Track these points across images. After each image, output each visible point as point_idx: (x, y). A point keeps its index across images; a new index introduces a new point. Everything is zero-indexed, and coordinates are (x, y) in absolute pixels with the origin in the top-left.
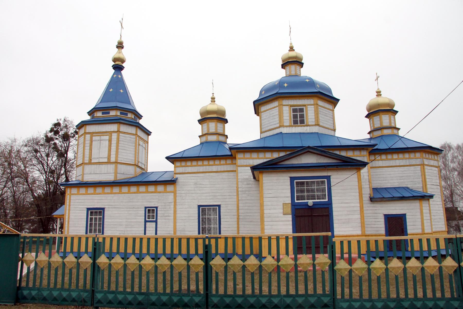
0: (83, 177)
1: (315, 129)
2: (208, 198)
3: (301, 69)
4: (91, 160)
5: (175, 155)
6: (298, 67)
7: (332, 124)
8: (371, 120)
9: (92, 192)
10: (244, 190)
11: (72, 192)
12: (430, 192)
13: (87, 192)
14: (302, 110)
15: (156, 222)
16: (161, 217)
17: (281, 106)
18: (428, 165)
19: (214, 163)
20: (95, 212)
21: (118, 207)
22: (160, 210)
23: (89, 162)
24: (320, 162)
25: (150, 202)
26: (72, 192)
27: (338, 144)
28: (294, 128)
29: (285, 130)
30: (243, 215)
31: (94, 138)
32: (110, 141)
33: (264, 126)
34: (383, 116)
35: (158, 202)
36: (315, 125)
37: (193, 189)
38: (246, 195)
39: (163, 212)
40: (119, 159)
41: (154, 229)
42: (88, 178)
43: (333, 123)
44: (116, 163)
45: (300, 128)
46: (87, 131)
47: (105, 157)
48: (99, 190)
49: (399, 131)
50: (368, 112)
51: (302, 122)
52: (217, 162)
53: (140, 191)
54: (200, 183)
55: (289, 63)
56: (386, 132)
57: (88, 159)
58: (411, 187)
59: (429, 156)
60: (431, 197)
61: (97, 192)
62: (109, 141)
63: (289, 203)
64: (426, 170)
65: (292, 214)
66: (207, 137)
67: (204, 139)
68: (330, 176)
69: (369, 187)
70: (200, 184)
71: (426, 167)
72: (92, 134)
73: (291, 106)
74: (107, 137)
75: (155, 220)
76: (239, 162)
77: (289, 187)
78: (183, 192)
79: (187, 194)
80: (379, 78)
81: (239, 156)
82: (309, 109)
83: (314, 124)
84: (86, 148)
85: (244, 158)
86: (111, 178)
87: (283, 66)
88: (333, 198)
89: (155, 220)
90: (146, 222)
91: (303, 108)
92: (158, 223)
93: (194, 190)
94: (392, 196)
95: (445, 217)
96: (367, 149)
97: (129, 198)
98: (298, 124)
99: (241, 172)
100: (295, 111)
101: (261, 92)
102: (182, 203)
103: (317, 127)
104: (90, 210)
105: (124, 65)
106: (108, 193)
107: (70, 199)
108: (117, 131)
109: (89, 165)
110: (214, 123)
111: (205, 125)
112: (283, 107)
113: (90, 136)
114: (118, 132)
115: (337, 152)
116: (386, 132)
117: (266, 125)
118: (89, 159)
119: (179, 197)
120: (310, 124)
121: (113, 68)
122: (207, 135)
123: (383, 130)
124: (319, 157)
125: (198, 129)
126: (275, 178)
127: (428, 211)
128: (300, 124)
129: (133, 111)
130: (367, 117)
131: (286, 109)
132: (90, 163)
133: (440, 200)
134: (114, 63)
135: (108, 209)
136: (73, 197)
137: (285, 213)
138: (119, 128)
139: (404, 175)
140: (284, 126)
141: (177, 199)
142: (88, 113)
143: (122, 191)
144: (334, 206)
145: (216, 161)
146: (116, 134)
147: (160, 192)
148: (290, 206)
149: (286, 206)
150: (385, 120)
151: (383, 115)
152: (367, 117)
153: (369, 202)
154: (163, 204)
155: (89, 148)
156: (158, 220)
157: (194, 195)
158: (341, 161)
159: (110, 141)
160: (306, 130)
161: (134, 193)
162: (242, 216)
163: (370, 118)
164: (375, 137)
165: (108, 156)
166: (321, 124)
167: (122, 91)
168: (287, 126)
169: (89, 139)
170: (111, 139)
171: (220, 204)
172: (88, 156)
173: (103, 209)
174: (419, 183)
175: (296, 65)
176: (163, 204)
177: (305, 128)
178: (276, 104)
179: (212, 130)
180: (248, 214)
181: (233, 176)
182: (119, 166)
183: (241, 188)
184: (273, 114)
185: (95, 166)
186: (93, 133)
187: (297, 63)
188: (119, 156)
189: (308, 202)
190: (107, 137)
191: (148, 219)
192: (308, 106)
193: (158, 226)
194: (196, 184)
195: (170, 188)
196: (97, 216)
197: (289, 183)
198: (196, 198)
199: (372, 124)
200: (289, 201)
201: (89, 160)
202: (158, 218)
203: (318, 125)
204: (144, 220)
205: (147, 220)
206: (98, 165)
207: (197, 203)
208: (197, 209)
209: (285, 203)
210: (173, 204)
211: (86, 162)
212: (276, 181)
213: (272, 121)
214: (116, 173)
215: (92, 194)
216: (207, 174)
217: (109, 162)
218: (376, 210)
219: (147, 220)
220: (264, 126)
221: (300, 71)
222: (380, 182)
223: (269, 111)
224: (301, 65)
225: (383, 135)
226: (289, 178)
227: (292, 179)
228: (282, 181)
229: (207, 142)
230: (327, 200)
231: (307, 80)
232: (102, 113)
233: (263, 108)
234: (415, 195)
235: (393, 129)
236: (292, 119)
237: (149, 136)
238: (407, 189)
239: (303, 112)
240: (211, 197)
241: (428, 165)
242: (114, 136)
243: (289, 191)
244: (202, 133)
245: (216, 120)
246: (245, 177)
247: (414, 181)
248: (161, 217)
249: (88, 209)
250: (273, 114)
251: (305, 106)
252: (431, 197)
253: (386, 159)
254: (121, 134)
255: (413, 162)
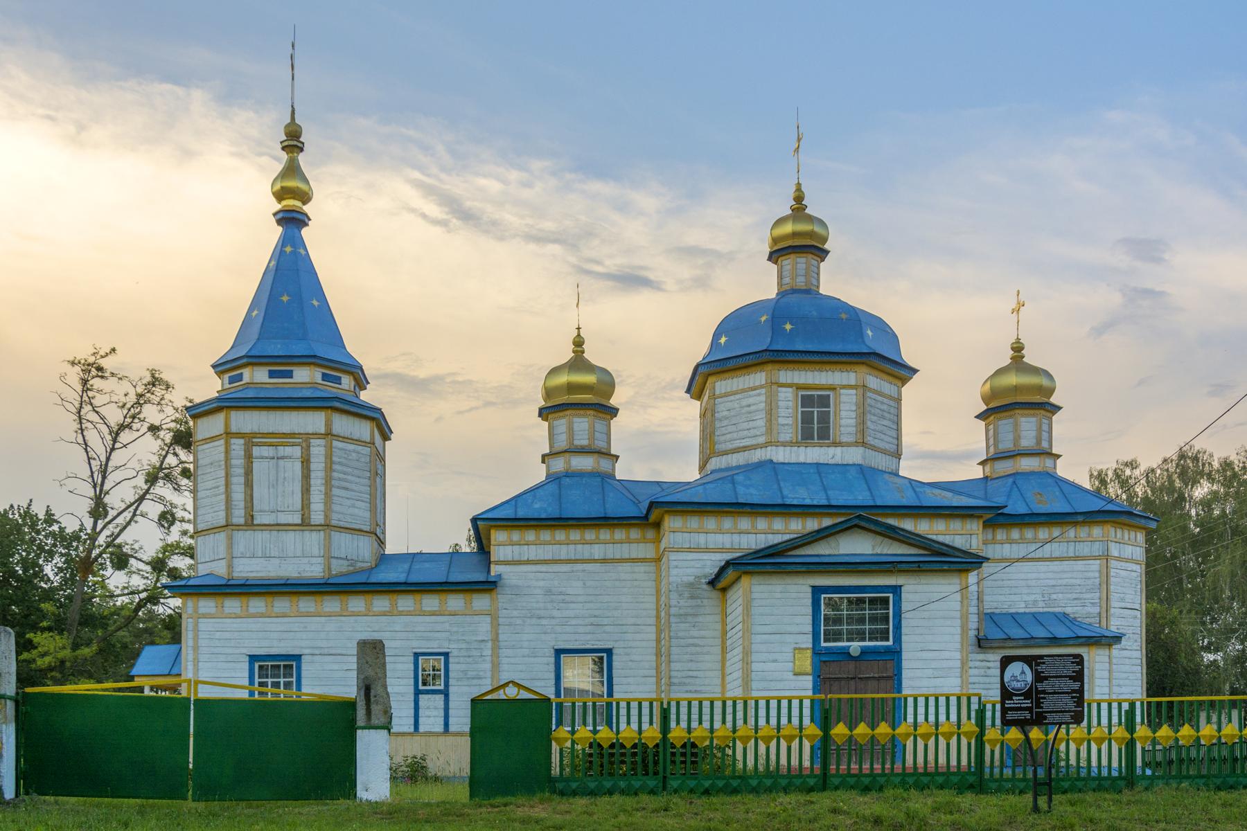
0: (230, 566)
1: (854, 455)
2: (581, 629)
3: (822, 264)
4: (252, 516)
5: (495, 511)
6: (812, 260)
7: (893, 438)
8: (991, 427)
9: (263, 610)
10: (682, 612)
11: (202, 611)
12: (1115, 626)
13: (247, 610)
14: (825, 402)
15: (447, 695)
16: (458, 679)
17: (774, 387)
18: (1119, 559)
19: (568, 537)
20: (284, 666)
21: (339, 651)
22: (456, 660)
23: (246, 522)
24: (885, 552)
25: (428, 639)
26: (202, 611)
27: (908, 499)
28: (802, 449)
29: (780, 455)
30: (679, 674)
31: (256, 451)
32: (306, 462)
33: (722, 438)
34: (1023, 419)
35: (450, 640)
36: (856, 444)
37: (541, 605)
38: (687, 625)
39: (463, 667)
40: (335, 516)
41: (442, 713)
42: (249, 569)
43: (896, 436)
44: (327, 526)
45: (817, 449)
46: (234, 429)
47: (295, 509)
48: (281, 604)
49: (1059, 461)
50: (987, 405)
51: (824, 434)
52: (605, 534)
53: (400, 609)
54: (560, 590)
55: (790, 251)
56: (1027, 464)
57: (242, 512)
58: (1074, 613)
59: (1123, 535)
60: (1117, 639)
61: (276, 610)
62: (302, 462)
63: (808, 649)
64: (1112, 570)
65: (813, 674)
66: (569, 460)
67: (559, 465)
68: (901, 586)
69: (976, 612)
70: (561, 594)
71: (1113, 563)
72: (251, 439)
73: (799, 387)
74: (297, 451)
75: (442, 687)
76: (669, 539)
77: (809, 610)
78: (515, 613)
79: (526, 619)
80: (1022, 308)
81: (670, 523)
82: (843, 398)
83: (851, 439)
84: (234, 480)
85: (685, 530)
86: (314, 570)
87: (774, 256)
88: (904, 638)
89: (442, 687)
90: (417, 693)
91: (829, 396)
92: (451, 695)
93: (546, 609)
94: (1029, 636)
95: (1145, 689)
96: (979, 517)
97: (368, 626)
98: (813, 439)
99: (677, 567)
100: (807, 401)
101: (717, 336)
102: (514, 643)
103: (860, 450)
104: (259, 661)
105: (306, 208)
106: (309, 615)
107: (196, 630)
108: (327, 434)
109: (249, 532)
110: (586, 419)
111: (561, 424)
112: (780, 389)
113: (245, 444)
114: (329, 434)
115: (908, 525)
116: (1027, 464)
117: (728, 436)
118: (245, 514)
119: (506, 627)
120: (844, 439)
121: (279, 222)
122: (567, 455)
123: (1018, 457)
124: (879, 538)
125: (539, 434)
126: (779, 588)
127: (1106, 674)
128: (818, 439)
129: (353, 370)
130: (981, 416)
131: (787, 395)
132: (250, 523)
133: (1136, 646)
134: (278, 207)
135: (310, 657)
136: (204, 625)
137: (797, 670)
138: (328, 424)
139: (1060, 582)
140: (778, 444)
141: (500, 632)
142: (214, 366)
143: (350, 609)
144: (904, 656)
145: (602, 531)
146: (322, 442)
147: (353, 614)
148: (809, 653)
149: (800, 656)
150: (1027, 425)
151: (1022, 416)
152: (981, 416)
153: (976, 649)
154: (464, 646)
155: (242, 480)
156: (451, 689)
157: (544, 622)
158: (926, 553)
159: (306, 462)
160: (831, 456)
161: (384, 614)
162: (676, 677)
163: (988, 421)
164: (997, 476)
165: (302, 507)
166: (869, 440)
167: (315, 303)
168: (784, 444)
169: (243, 453)
170: (309, 455)
171: (610, 647)
172: (242, 504)
173: (298, 658)
174: (1092, 603)
175: (810, 256)
176: (464, 646)
177: (831, 450)
178: (758, 378)
179: (580, 440)
180: (691, 673)
181: (645, 572)
182: (337, 537)
183: (675, 606)
184: (749, 406)
185: (266, 535)
186: (255, 435)
187: (813, 251)
188: (336, 508)
189: (849, 647)
190: (297, 451)
191: (424, 684)
192: (842, 391)
193: (451, 705)
194: (550, 591)
195: (481, 602)
196: (280, 678)
197: (808, 601)
198: (549, 631)
199: (993, 438)
200: (807, 642)
201: (245, 516)
202: (451, 682)
203: (864, 444)
204: (411, 689)
205: (421, 687)
206: (275, 533)
207: (552, 644)
208: (552, 660)
209: (800, 649)
210: (489, 644)
211: (235, 521)
212: (779, 595)
213: (745, 425)
214: (328, 557)
215: (262, 616)
216: (579, 567)
217: (305, 524)
218: (989, 668)
219: (421, 687)
220: (722, 438)
221: (818, 268)
222: (1002, 598)
223: (738, 396)
224: (822, 253)
225: (1017, 473)
226: (810, 590)
227: (817, 591)
228: (794, 595)
229: (568, 474)
230: (890, 643)
231: (844, 316)
232: (270, 371)
233: (722, 385)
234: (1080, 635)
235: (1042, 457)
236: (800, 425)
237: (387, 442)
238: (1063, 618)
239: (829, 407)
240: (589, 629)
241: (1119, 559)
242: (318, 449)
243: (809, 619)
244: (551, 447)
245: (592, 412)
246: (685, 579)
247: (1081, 599)
248: (458, 679)
249: (253, 658)
250: (749, 406)
251: (833, 388)
252: (1117, 639)
253: (1020, 541)
254: (335, 443)
255: (1084, 549)
